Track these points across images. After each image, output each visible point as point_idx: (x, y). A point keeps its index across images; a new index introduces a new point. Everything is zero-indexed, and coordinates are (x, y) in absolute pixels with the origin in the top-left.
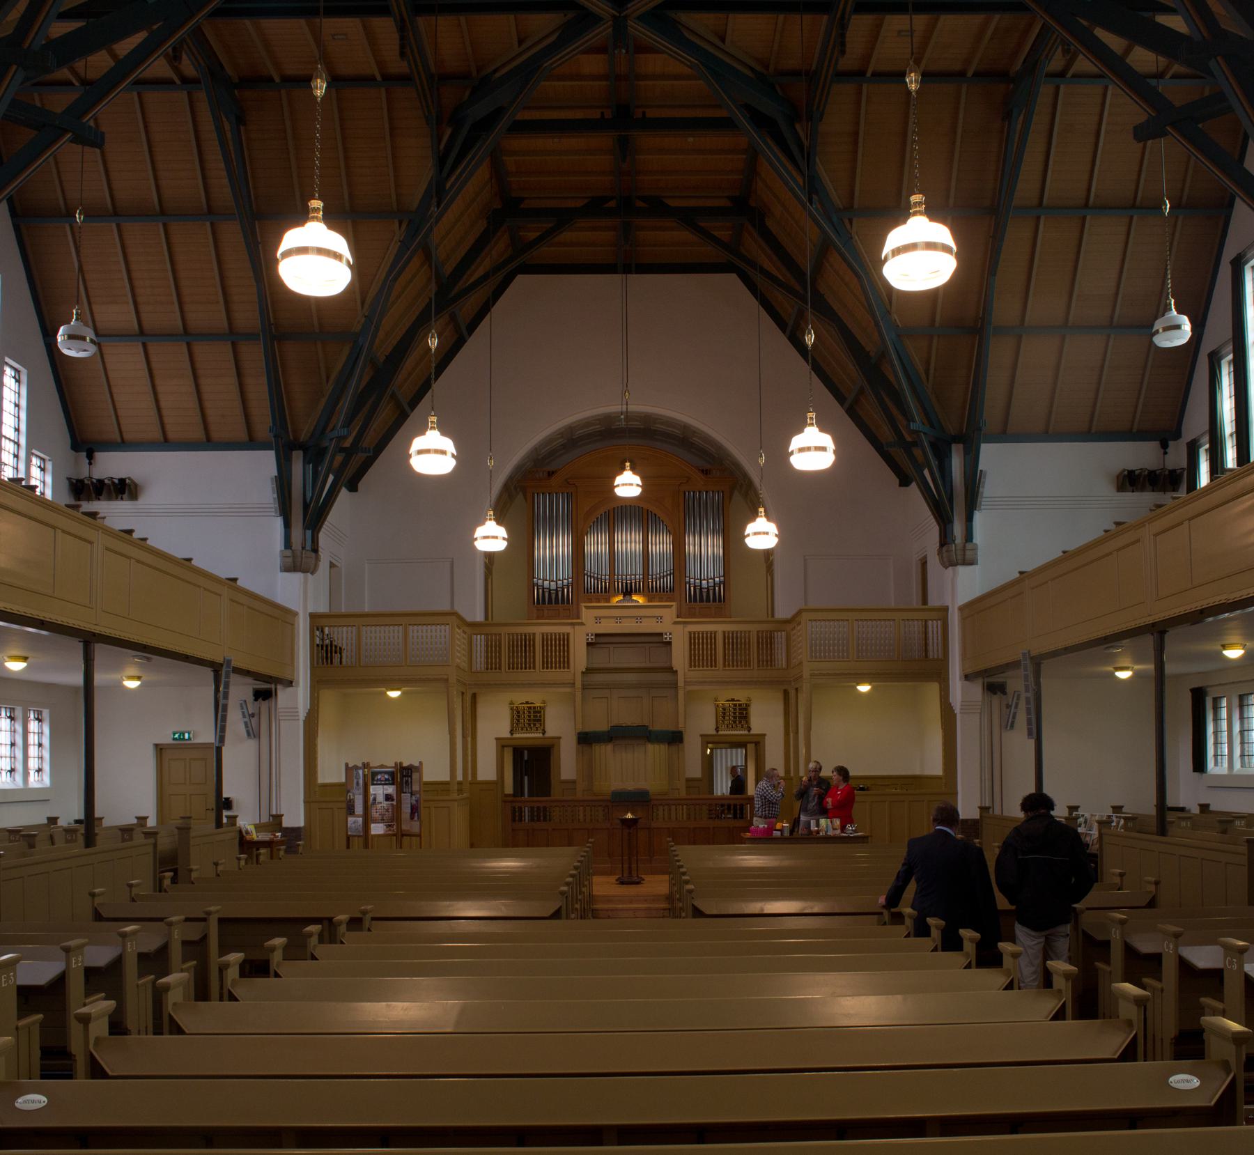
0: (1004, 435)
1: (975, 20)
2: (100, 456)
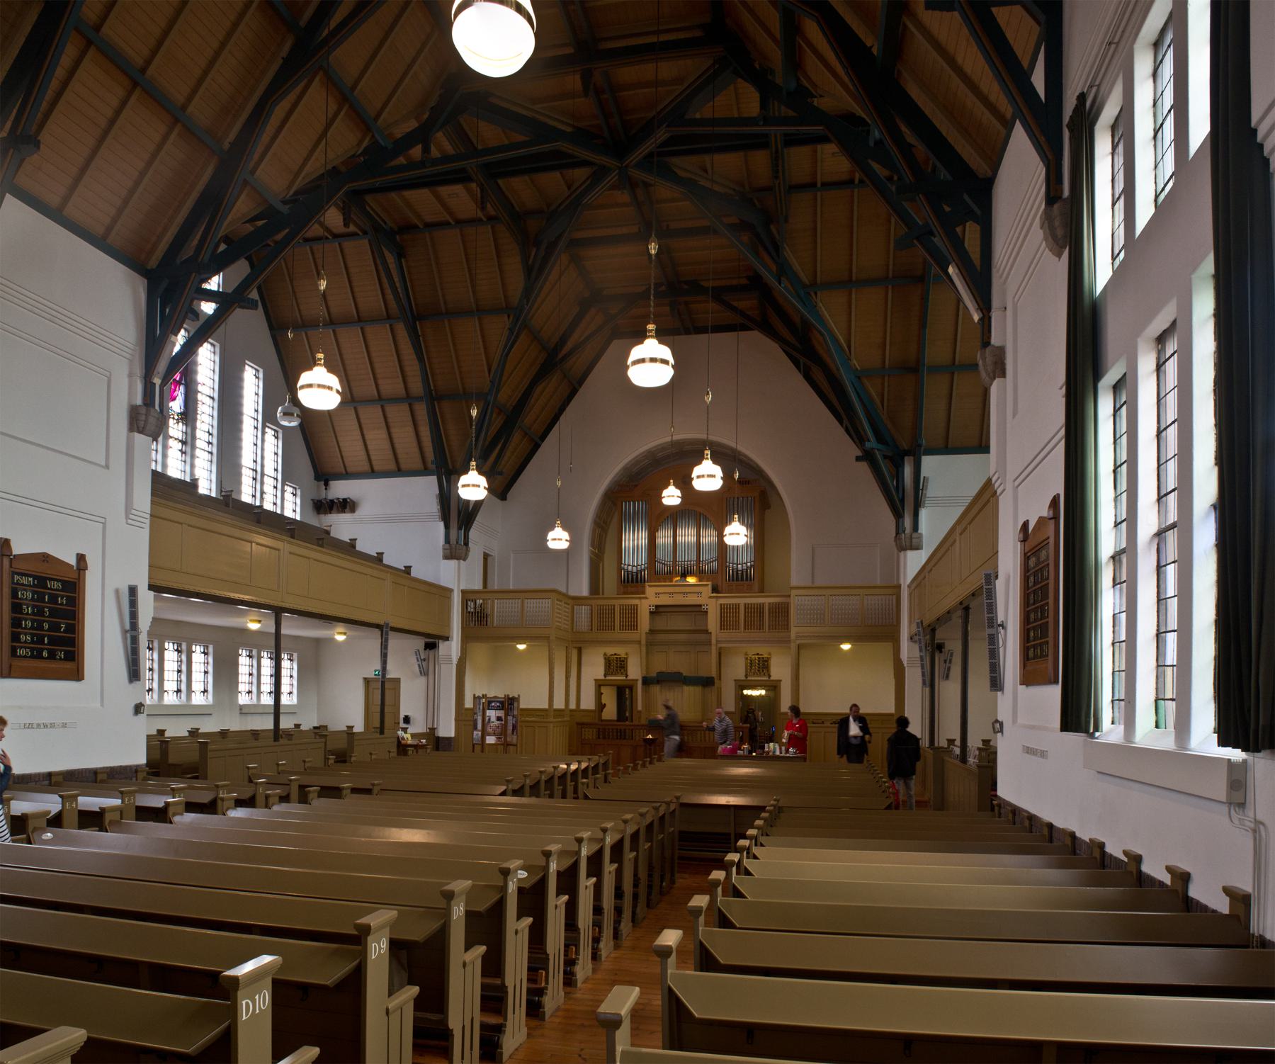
2: (333, 484)
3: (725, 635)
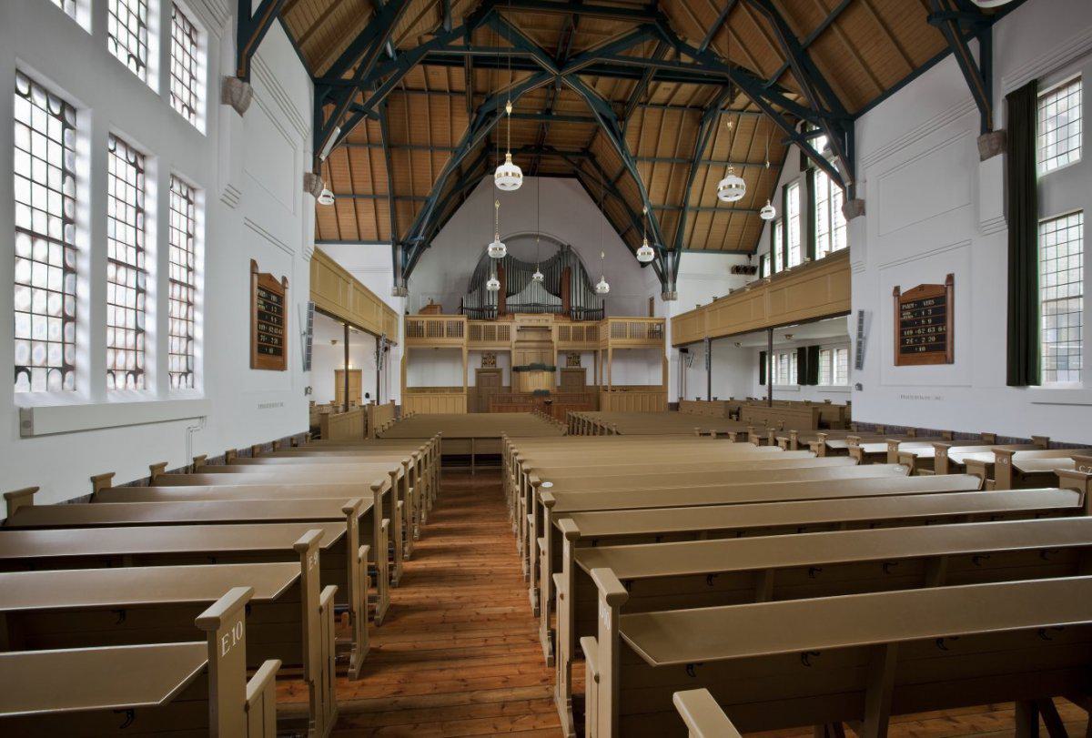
0: (689, 249)
1: (695, 86)
3: (562, 343)
